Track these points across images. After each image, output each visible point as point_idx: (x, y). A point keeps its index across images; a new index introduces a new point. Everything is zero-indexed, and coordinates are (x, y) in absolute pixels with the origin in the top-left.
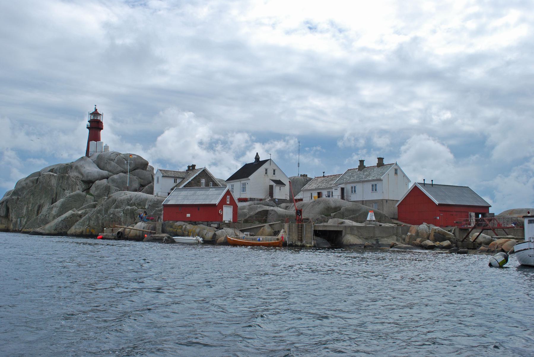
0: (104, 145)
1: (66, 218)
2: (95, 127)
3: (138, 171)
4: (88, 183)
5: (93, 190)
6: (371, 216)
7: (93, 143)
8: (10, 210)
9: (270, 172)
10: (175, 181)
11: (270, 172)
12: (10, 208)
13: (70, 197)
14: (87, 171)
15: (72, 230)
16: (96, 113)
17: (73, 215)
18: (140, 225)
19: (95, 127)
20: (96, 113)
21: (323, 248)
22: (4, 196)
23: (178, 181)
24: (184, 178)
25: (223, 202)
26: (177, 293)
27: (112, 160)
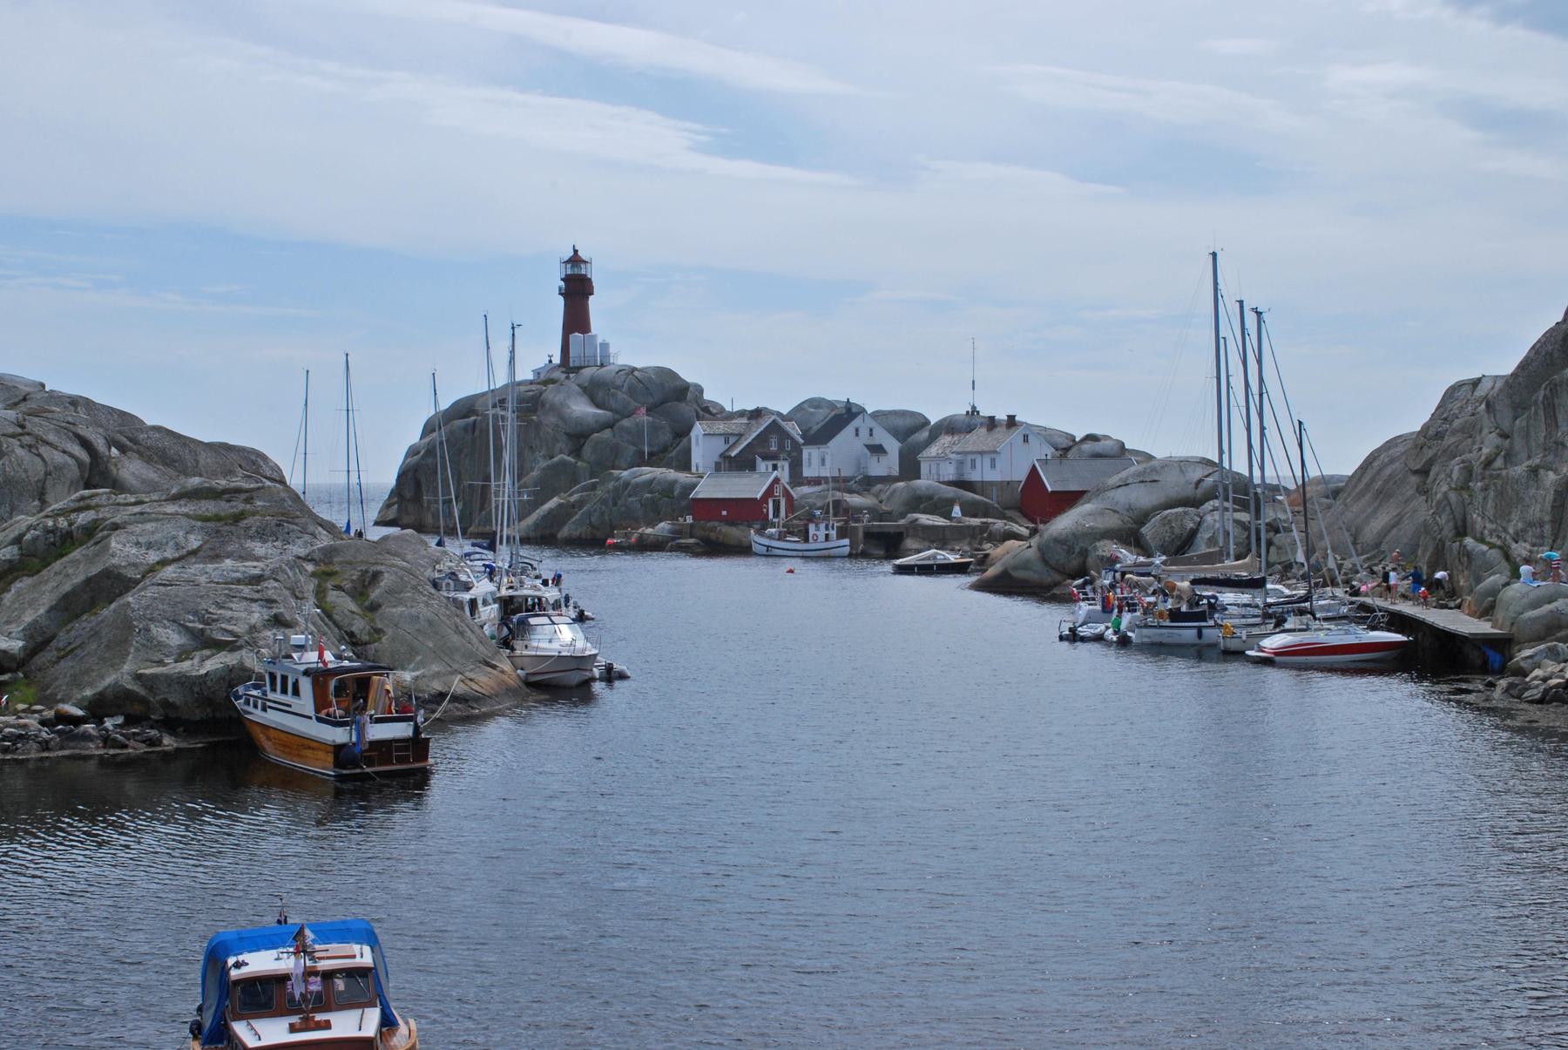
0: (599, 341)
1: (551, 511)
2: (577, 289)
3: (670, 403)
4: (578, 437)
5: (587, 450)
6: (957, 511)
7: (576, 337)
8: (424, 488)
9: (864, 433)
10: (727, 441)
11: (864, 433)
12: (423, 480)
13: (549, 467)
14: (575, 415)
15: (564, 532)
16: (575, 260)
17: (561, 505)
18: (664, 527)
19: (577, 289)
20: (575, 260)
21: (877, 558)
22: (407, 457)
23: (732, 440)
24: (740, 435)
25: (769, 492)
26: (497, 478)
27: (619, 388)
